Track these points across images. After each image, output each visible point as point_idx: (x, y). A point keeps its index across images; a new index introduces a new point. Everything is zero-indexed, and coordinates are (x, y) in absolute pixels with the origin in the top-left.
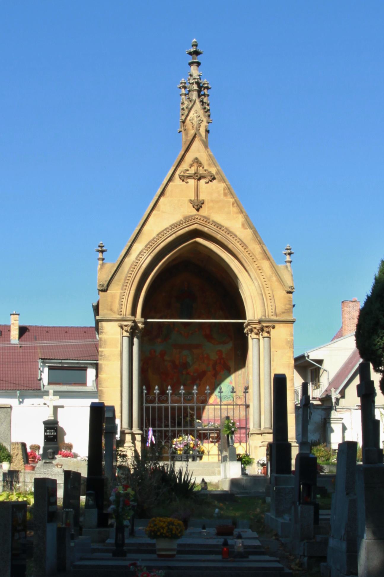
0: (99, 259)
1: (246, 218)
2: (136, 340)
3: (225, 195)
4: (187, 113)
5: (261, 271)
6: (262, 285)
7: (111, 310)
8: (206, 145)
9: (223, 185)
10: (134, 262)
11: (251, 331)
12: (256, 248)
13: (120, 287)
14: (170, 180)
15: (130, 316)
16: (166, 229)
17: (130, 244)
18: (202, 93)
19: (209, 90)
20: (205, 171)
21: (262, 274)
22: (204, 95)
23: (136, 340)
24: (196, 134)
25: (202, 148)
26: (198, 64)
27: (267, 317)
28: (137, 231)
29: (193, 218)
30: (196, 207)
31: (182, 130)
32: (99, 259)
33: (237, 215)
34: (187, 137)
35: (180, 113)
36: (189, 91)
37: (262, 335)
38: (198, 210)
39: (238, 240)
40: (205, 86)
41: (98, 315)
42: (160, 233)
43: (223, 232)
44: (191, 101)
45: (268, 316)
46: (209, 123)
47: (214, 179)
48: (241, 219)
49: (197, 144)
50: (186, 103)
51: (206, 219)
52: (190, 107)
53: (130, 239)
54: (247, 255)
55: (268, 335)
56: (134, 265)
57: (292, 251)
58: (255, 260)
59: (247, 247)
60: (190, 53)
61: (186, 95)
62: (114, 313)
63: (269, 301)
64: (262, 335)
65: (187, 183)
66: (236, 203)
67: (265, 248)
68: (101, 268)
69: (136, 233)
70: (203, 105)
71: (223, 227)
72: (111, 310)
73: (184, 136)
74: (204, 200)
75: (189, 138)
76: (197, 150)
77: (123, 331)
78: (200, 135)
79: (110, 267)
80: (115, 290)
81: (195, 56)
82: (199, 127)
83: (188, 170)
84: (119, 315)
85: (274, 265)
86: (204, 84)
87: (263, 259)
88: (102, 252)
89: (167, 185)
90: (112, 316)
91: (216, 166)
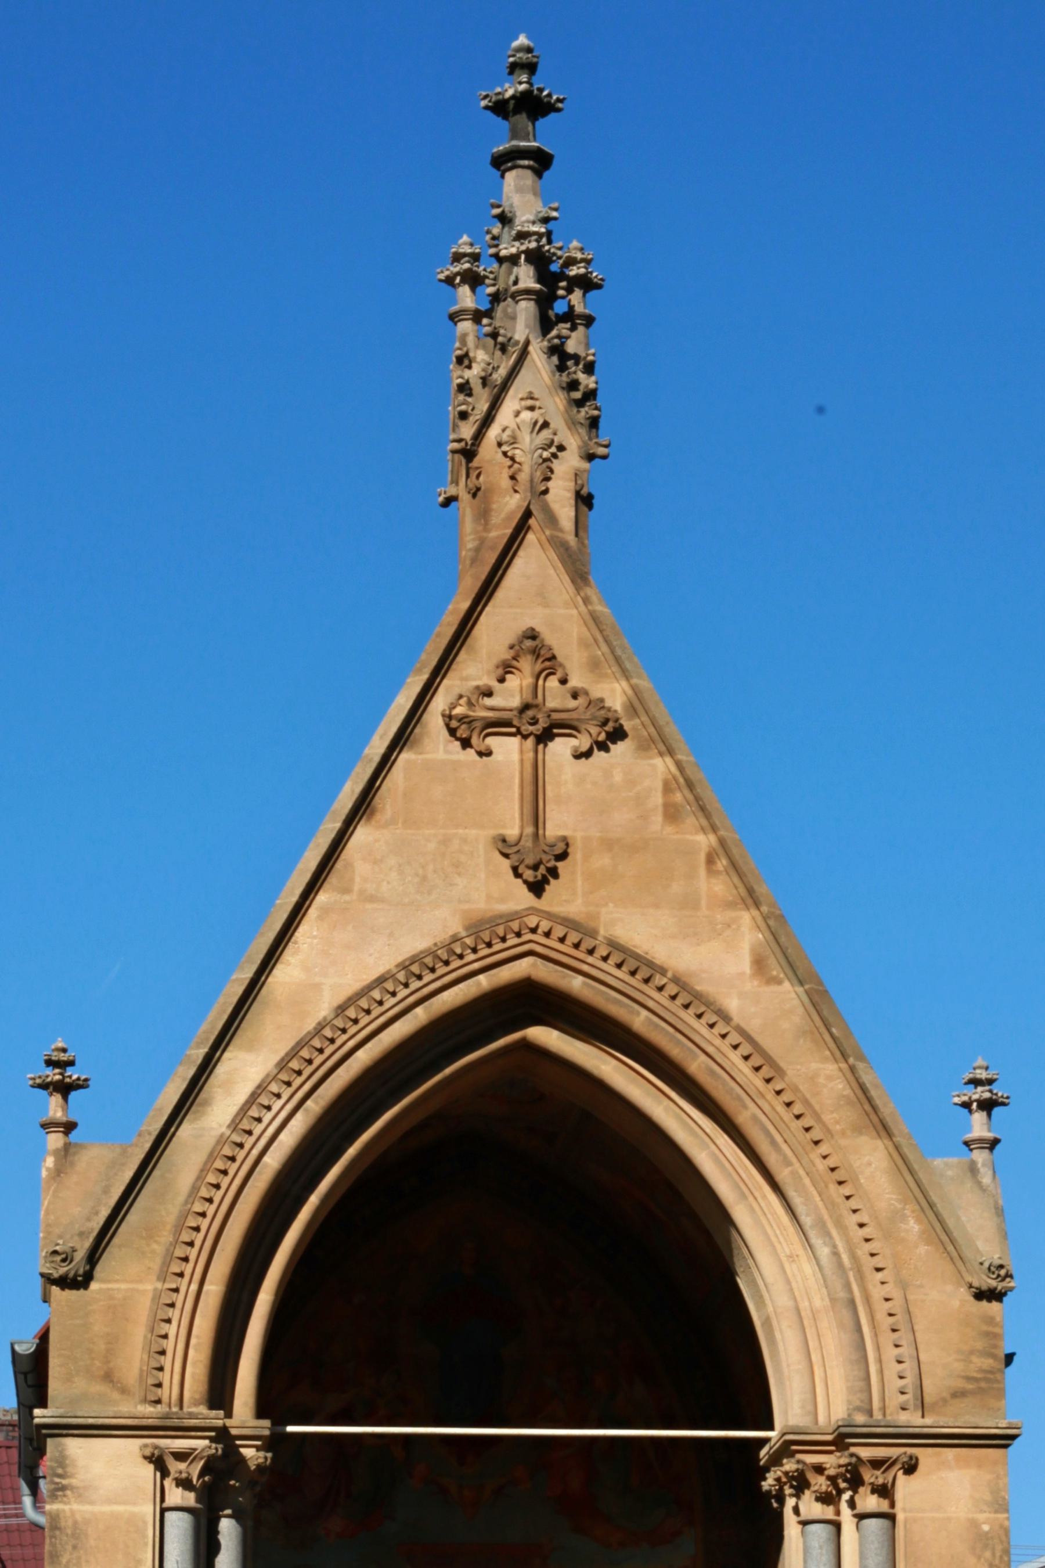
0: (47, 1126)
1: (777, 929)
2: (228, 1529)
3: (672, 814)
4: (483, 406)
5: (846, 1190)
6: (854, 1257)
7: (108, 1377)
8: (577, 569)
9: (661, 766)
10: (222, 1141)
11: (800, 1484)
12: (820, 1077)
13: (156, 1264)
14: (401, 740)
15: (203, 1410)
16: (381, 980)
17: (203, 1051)
18: (560, 307)
19: (593, 294)
20: (575, 696)
21: (853, 1204)
22: (570, 316)
23: (228, 1529)
24: (528, 514)
25: (559, 583)
26: (541, 162)
27: (877, 1415)
28: (239, 990)
29: (515, 926)
30: (529, 875)
31: (461, 490)
32: (47, 1126)
33: (731, 914)
34: (486, 527)
35: (452, 411)
36: (496, 298)
37: (852, 1504)
38: (537, 888)
39: (734, 1038)
40: (574, 271)
41: (43, 1403)
42: (351, 1001)
43: (662, 998)
44: (503, 349)
45: (883, 1409)
46: (590, 457)
47: (618, 734)
48: (748, 933)
49: (533, 561)
50: (481, 356)
51: (580, 934)
52: (499, 376)
53: (204, 1027)
54: (781, 1109)
55: (884, 1506)
56: (227, 1152)
57: (999, 1090)
58: (815, 1134)
59: (780, 1072)
60: (500, 108)
61: (477, 316)
62: (124, 1391)
63: (887, 1339)
64: (852, 1504)
65: (486, 753)
66: (726, 856)
67: (867, 1079)
68: (58, 1172)
69: (235, 1000)
70: (561, 368)
71: (663, 971)
72: (108, 1377)
73: (469, 525)
74: (566, 841)
75: (493, 534)
76: (536, 594)
77: (167, 1483)
78: (552, 519)
79: (102, 1168)
80: (129, 1279)
81: (522, 119)
82: (547, 479)
83: (489, 694)
84: (144, 1400)
85: (911, 1156)
86: (571, 262)
87: (858, 1130)
88: (65, 1089)
89: (386, 762)
90: (111, 1410)
91: (626, 674)
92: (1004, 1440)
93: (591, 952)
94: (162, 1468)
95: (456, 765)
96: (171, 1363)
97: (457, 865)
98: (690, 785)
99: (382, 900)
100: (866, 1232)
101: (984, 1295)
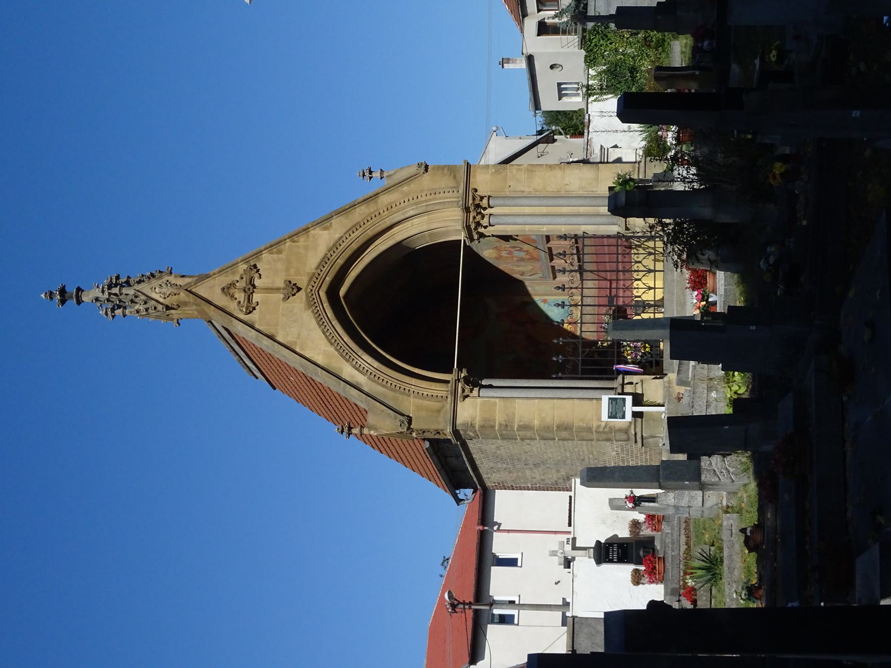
3: (280, 252)
9: (265, 255)
10: (369, 378)
13: (405, 397)
16: (324, 333)
23: (484, 382)
25: (209, 282)
38: (299, 289)
39: (347, 235)
42: (329, 341)
47: (255, 266)
48: (317, 232)
50: (137, 307)
51: (312, 277)
56: (373, 377)
59: (359, 223)
60: (63, 302)
62: (443, 407)
66: (293, 237)
68: (375, 429)
72: (439, 411)
76: (211, 290)
87: (377, 202)
92: (468, 166)
94: (468, 396)
96: (435, 393)
98: (271, 246)
101: (426, 170)
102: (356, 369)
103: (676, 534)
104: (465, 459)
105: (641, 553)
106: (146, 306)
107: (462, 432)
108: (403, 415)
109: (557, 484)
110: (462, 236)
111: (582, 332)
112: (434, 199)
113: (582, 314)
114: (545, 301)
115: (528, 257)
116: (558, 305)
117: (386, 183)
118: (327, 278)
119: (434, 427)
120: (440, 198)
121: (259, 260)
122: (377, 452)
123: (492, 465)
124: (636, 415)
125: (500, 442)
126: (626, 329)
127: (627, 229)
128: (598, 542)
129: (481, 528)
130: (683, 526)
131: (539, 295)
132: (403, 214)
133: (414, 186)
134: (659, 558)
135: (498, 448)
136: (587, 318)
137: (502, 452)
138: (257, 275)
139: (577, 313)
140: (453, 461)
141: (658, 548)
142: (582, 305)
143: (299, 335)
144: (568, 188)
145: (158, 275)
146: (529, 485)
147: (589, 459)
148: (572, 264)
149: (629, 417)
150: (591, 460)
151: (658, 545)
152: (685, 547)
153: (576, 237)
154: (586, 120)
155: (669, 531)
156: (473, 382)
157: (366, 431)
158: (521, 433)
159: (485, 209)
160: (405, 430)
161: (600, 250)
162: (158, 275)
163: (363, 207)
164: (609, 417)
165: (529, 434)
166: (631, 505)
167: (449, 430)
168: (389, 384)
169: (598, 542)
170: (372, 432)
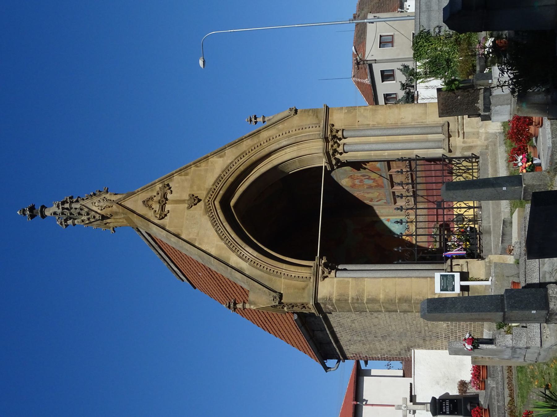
3: (187, 174)
9: (176, 178)
13: (278, 278)
16: (216, 231)
20: (158, 194)
23: (340, 267)
24: (117, 203)
26: (43, 207)
33: (209, 163)
46: (107, 192)
47: (168, 185)
48: (215, 159)
49: (128, 203)
56: (253, 264)
60: (32, 216)
62: (307, 285)
68: (255, 304)
71: (221, 175)
78: (120, 200)
83: (156, 211)
87: (259, 137)
92: (327, 108)
93: (215, 189)
94: (327, 277)
95: (170, 217)
97: (192, 217)
99: (199, 232)
100: (281, 134)
102: (240, 257)
103: (500, 387)
104: (328, 332)
105: (469, 407)
106: (88, 217)
107: (322, 306)
108: (276, 292)
109: (400, 354)
110: (323, 163)
111: (416, 242)
112: (301, 133)
113: (416, 228)
114: (388, 220)
115: (375, 184)
116: (397, 222)
117: (267, 124)
118: (221, 192)
119: (300, 301)
120: (306, 132)
121: (171, 181)
122: (267, 332)
123: (349, 337)
124: (464, 288)
125: (354, 316)
126: (457, 189)
127: (450, 151)
128: (434, 398)
129: (355, 403)
130: (506, 381)
131: (384, 216)
132: (278, 144)
133: (286, 124)
134: (485, 410)
135: (353, 321)
136: (420, 219)
137: (356, 325)
138: (169, 191)
139: (413, 228)
140: (319, 335)
141: (482, 403)
142: (416, 235)
143: (198, 234)
144: (403, 121)
145: (98, 193)
146: (379, 356)
147: (425, 330)
148: (408, 190)
149: (457, 290)
150: (427, 332)
151: (482, 401)
152: (509, 399)
153: (410, 160)
154: (416, 95)
155: (495, 386)
156: (332, 265)
157: (247, 306)
158: (370, 305)
159: (340, 139)
160: (277, 304)
161: (428, 173)
162: (98, 193)
163: (249, 140)
164: (441, 290)
165: (376, 306)
166: (469, 347)
167: (311, 303)
168: (265, 269)
169: (434, 398)
170: (252, 307)
